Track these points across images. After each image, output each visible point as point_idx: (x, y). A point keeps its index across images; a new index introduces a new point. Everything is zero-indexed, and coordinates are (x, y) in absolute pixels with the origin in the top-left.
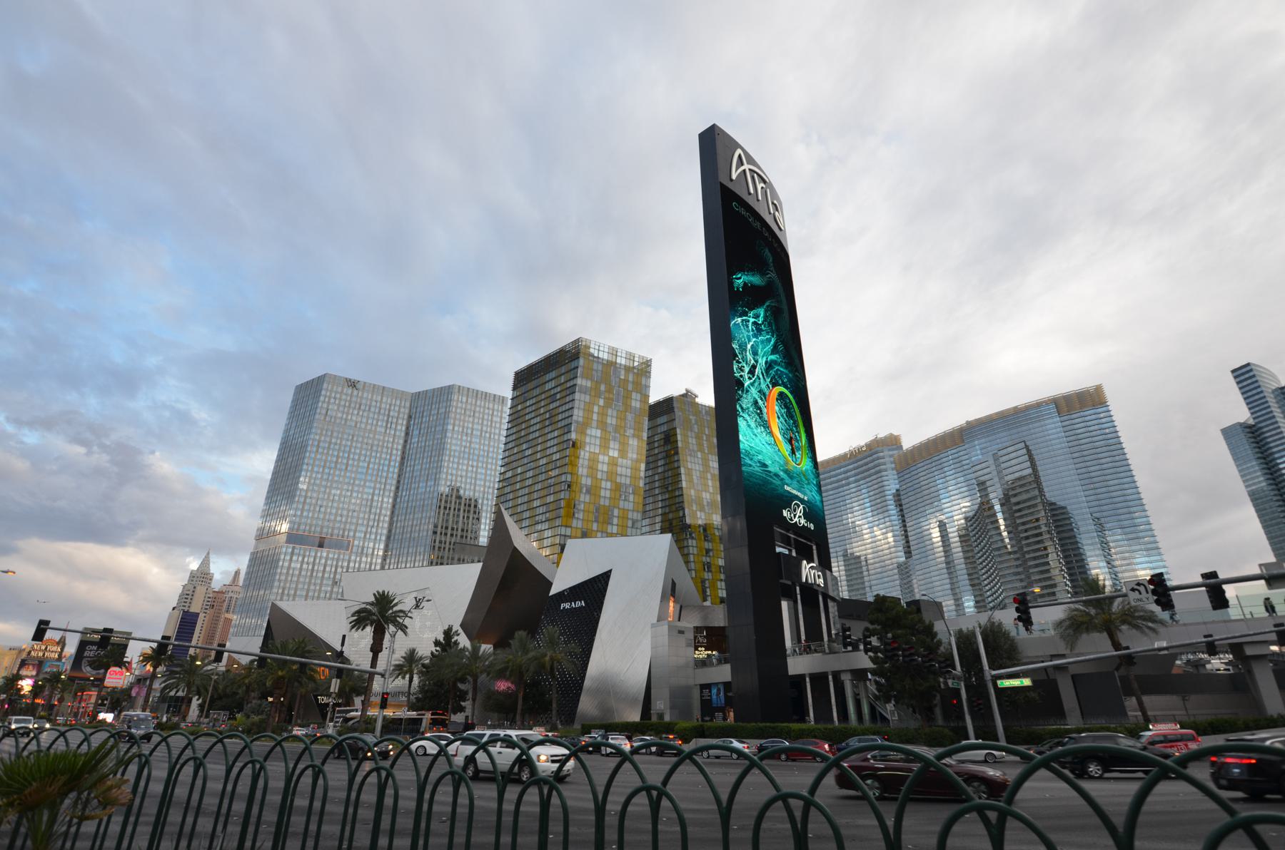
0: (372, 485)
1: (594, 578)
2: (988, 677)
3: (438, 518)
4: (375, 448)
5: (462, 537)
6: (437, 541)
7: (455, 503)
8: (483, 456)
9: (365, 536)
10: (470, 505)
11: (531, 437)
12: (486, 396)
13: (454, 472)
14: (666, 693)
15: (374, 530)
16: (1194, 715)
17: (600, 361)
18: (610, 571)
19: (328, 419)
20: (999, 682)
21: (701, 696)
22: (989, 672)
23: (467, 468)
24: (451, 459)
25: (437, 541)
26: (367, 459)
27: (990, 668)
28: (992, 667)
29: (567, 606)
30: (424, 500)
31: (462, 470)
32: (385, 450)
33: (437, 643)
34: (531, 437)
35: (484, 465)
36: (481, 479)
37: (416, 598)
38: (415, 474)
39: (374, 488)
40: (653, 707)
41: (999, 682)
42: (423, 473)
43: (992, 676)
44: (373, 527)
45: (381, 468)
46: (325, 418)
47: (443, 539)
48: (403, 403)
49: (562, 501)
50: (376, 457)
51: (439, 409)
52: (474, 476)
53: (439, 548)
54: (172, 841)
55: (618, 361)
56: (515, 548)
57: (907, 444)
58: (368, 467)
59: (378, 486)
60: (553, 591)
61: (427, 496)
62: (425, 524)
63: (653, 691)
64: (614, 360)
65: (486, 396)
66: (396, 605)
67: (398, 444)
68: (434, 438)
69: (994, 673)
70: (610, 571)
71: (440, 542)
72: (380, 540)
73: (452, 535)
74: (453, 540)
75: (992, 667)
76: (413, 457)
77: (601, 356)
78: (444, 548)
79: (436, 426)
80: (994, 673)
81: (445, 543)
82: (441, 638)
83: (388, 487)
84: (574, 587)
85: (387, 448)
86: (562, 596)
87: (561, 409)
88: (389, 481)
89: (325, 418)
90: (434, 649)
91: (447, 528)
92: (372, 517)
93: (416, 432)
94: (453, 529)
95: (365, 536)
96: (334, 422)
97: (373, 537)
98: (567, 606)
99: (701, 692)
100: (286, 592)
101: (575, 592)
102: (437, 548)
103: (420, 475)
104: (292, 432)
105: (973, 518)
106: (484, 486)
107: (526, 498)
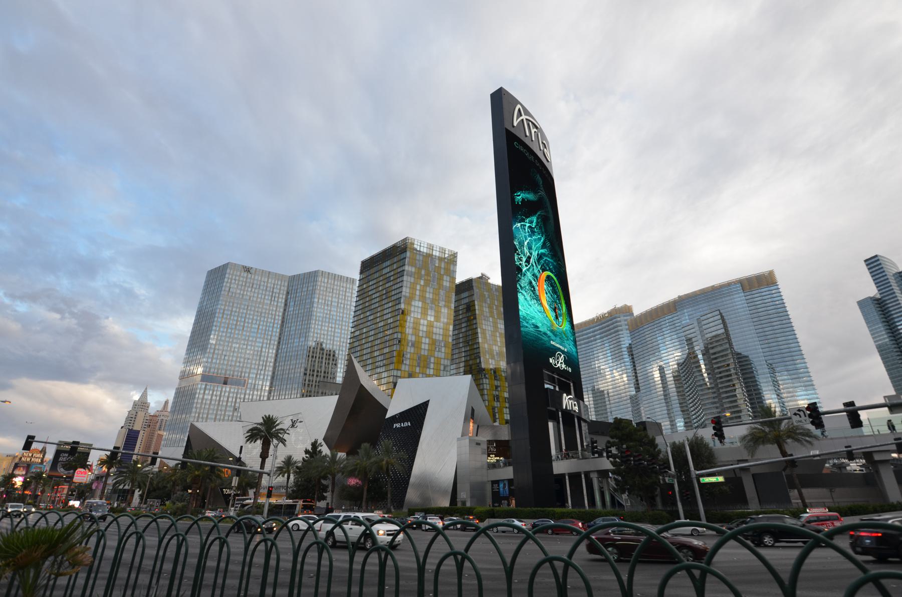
0: (261, 341)
1: (417, 406)
2: (693, 476)
4: (263, 315)
5: (324, 377)
6: (307, 380)
7: (320, 353)
9: (256, 376)
11: (373, 307)
12: (341, 278)
13: (319, 331)
14: (467, 487)
15: (263, 372)
17: (421, 253)
18: (428, 401)
19: (230, 294)
20: (701, 479)
21: (492, 489)
22: (694, 472)
23: (328, 329)
24: (317, 322)
25: (307, 380)
27: (695, 469)
28: (696, 469)
29: (398, 425)
30: (298, 351)
32: (270, 316)
33: (307, 452)
34: (373, 307)
35: (340, 327)
36: (337, 337)
37: (292, 420)
38: (291, 333)
39: (263, 343)
40: (458, 496)
41: (701, 479)
42: (297, 332)
43: (697, 475)
44: (262, 370)
45: (267, 329)
46: (228, 294)
47: (311, 379)
48: (283, 283)
49: (395, 352)
50: (264, 321)
51: (308, 287)
52: (333, 334)
53: (308, 385)
55: (434, 254)
56: (362, 385)
58: (258, 328)
59: (265, 341)
60: (388, 415)
61: (300, 348)
62: (298, 368)
63: (458, 485)
64: (431, 253)
65: (341, 278)
67: (279, 312)
68: (304, 308)
69: (698, 472)
70: (428, 401)
71: (309, 381)
72: (267, 379)
74: (318, 380)
75: (696, 469)
76: (290, 321)
77: (422, 250)
78: (312, 385)
79: (306, 299)
80: (698, 472)
81: (312, 381)
82: (310, 448)
83: (272, 342)
84: (403, 412)
86: (394, 419)
87: (394, 288)
88: (273, 338)
89: (228, 294)
90: (304, 456)
91: (314, 371)
92: (261, 363)
93: (292, 304)
94: (318, 371)
95: (256, 376)
97: (262, 377)
98: (398, 425)
99: (492, 486)
100: (201, 416)
101: (403, 416)
103: (295, 334)
104: (205, 304)
106: (340, 341)
107: (369, 350)
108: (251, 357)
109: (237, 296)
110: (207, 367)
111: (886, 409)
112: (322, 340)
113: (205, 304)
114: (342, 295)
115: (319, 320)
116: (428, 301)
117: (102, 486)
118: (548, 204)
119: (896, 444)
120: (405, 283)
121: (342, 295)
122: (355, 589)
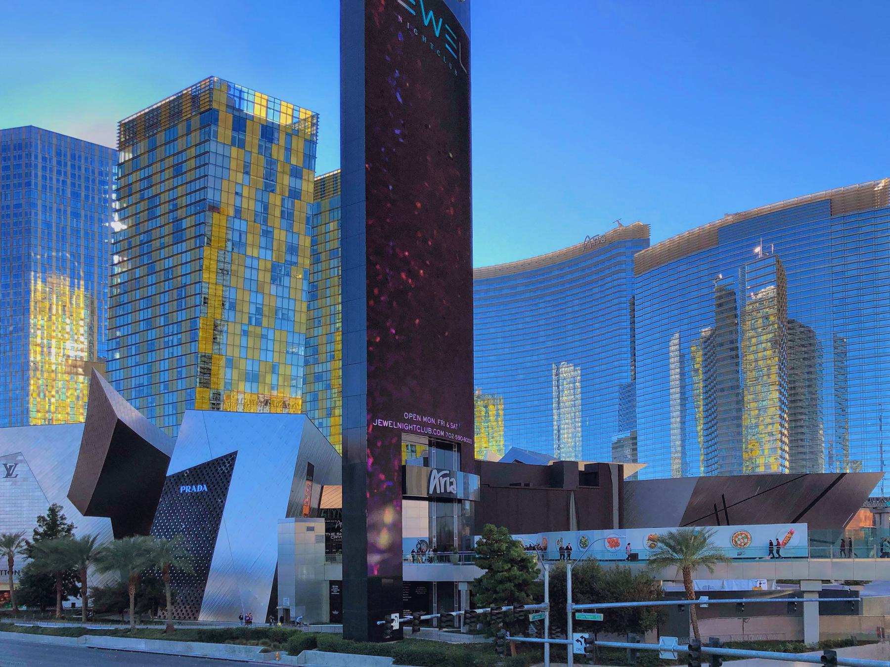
1: (217, 460)
14: (292, 590)
16: (748, 635)
20: (577, 614)
21: (331, 592)
22: (571, 606)
27: (573, 601)
29: (187, 489)
33: (41, 519)
37: (5, 465)
41: (577, 614)
54: (154, 135)
56: (119, 420)
57: (659, 238)
60: (172, 470)
75: (576, 601)
82: (45, 513)
84: (195, 468)
86: (180, 478)
90: (36, 524)
98: (187, 489)
99: (331, 588)
101: (196, 474)
105: (709, 339)
111: (466, 584)
117: (118, 619)
119: (819, 602)
120: (211, 179)
122: (2, 520)
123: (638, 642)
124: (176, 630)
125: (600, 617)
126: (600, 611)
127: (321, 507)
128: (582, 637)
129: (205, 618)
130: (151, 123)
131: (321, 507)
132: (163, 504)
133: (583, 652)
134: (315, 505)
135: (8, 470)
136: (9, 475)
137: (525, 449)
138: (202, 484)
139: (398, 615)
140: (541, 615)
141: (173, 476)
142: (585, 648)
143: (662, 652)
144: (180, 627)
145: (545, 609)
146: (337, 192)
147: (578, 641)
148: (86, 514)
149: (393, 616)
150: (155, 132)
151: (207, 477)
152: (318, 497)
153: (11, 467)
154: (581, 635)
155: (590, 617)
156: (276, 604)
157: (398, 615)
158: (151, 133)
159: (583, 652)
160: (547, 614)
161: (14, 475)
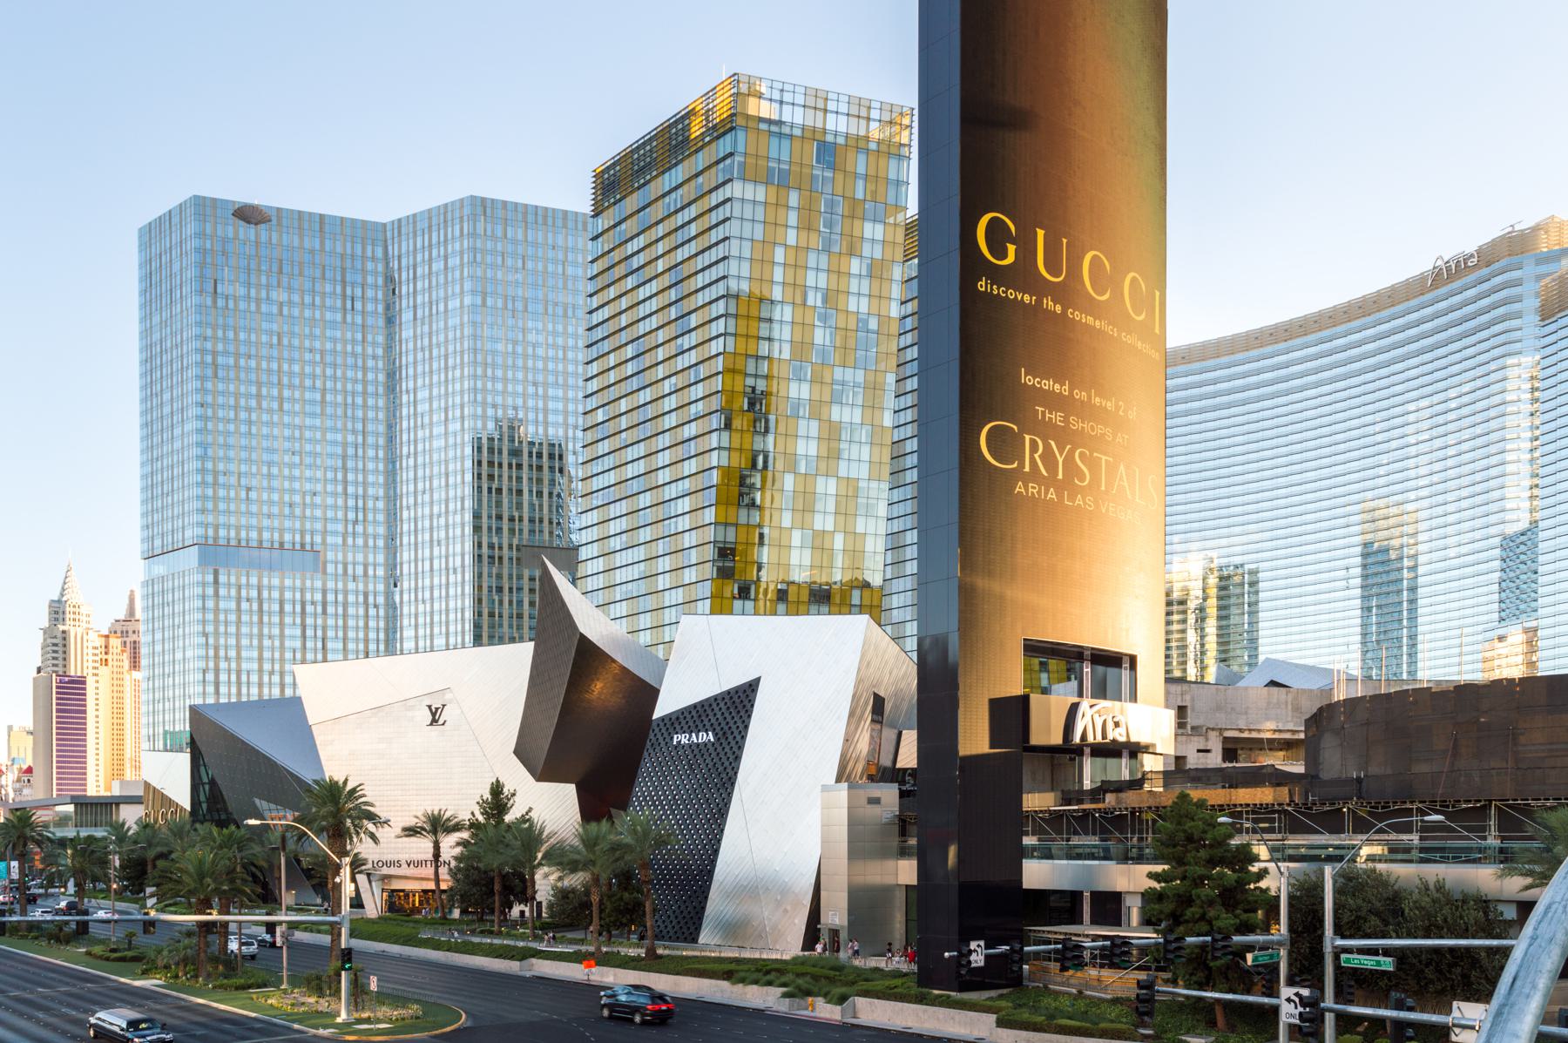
0: (339, 437)
2: (1328, 949)
3: (480, 501)
4: (329, 359)
5: (532, 532)
6: (485, 545)
7: (510, 466)
8: (556, 359)
9: (344, 541)
10: (540, 455)
11: (642, 328)
12: (545, 217)
13: (499, 400)
15: (360, 529)
17: (786, 130)
18: (758, 680)
19: (220, 303)
20: (1343, 956)
23: (525, 389)
24: (489, 372)
25: (485, 545)
26: (318, 384)
28: (1339, 931)
29: (683, 739)
30: (446, 462)
31: (515, 394)
32: (350, 361)
34: (642, 328)
35: (561, 380)
36: (556, 412)
37: (430, 707)
38: (419, 409)
39: (345, 445)
40: (823, 920)
41: (1343, 956)
42: (435, 405)
43: (1335, 947)
44: (356, 522)
45: (349, 400)
46: (215, 302)
47: (495, 540)
48: (369, 248)
49: (715, 472)
50: (335, 378)
51: (446, 258)
52: (541, 404)
53: (491, 557)
55: (830, 126)
56: (581, 635)
58: (323, 401)
59: (350, 438)
60: (660, 711)
61: (451, 454)
62: (455, 512)
63: (823, 894)
64: (819, 124)
65: (545, 217)
66: (361, 797)
67: (374, 344)
68: (446, 328)
69: (1340, 942)
70: (758, 680)
71: (491, 546)
72: (375, 546)
73: (512, 531)
74: (515, 542)
75: (1339, 931)
76: (411, 371)
77: (786, 118)
78: (500, 558)
79: (446, 299)
80: (1340, 942)
81: (500, 548)
83: (370, 440)
85: (354, 354)
87: (700, 262)
88: (370, 427)
89: (215, 302)
91: (499, 517)
92: (351, 503)
93: (407, 316)
94: (512, 519)
95: (344, 541)
96: (236, 309)
97: (360, 541)
98: (683, 739)
100: (222, 653)
102: (485, 559)
103: (431, 410)
104: (156, 337)
106: (566, 425)
107: (641, 467)
108: (319, 487)
109: (242, 305)
110: (206, 526)
112: (511, 413)
113: (156, 337)
114: (357, 640)
115: (494, 366)
116: (814, 299)
118: (398, 930)
121: (357, 640)
123: (1410, 1009)
124: (661, 957)
125: (1387, 964)
126: (1387, 952)
127: (899, 765)
128: (1297, 994)
129: (709, 940)
130: (642, 164)
131: (899, 765)
132: (646, 765)
133: (1298, 1022)
134: (886, 761)
135: (434, 714)
136: (434, 721)
137: (1331, 667)
138: (706, 731)
139: (982, 943)
140: (1271, 956)
141: (662, 719)
142: (1301, 1013)
143: (1457, 1030)
144: (667, 952)
145: (1280, 943)
146: (1518, 299)
147: (1289, 1000)
148: (540, 777)
149: (973, 945)
150: (648, 177)
151: (713, 721)
152: (892, 750)
153: (437, 709)
154: (1295, 990)
155: (1368, 962)
156: (818, 922)
157: (982, 943)
158: (642, 181)
159: (1298, 1022)
160: (1283, 953)
161: (441, 722)
